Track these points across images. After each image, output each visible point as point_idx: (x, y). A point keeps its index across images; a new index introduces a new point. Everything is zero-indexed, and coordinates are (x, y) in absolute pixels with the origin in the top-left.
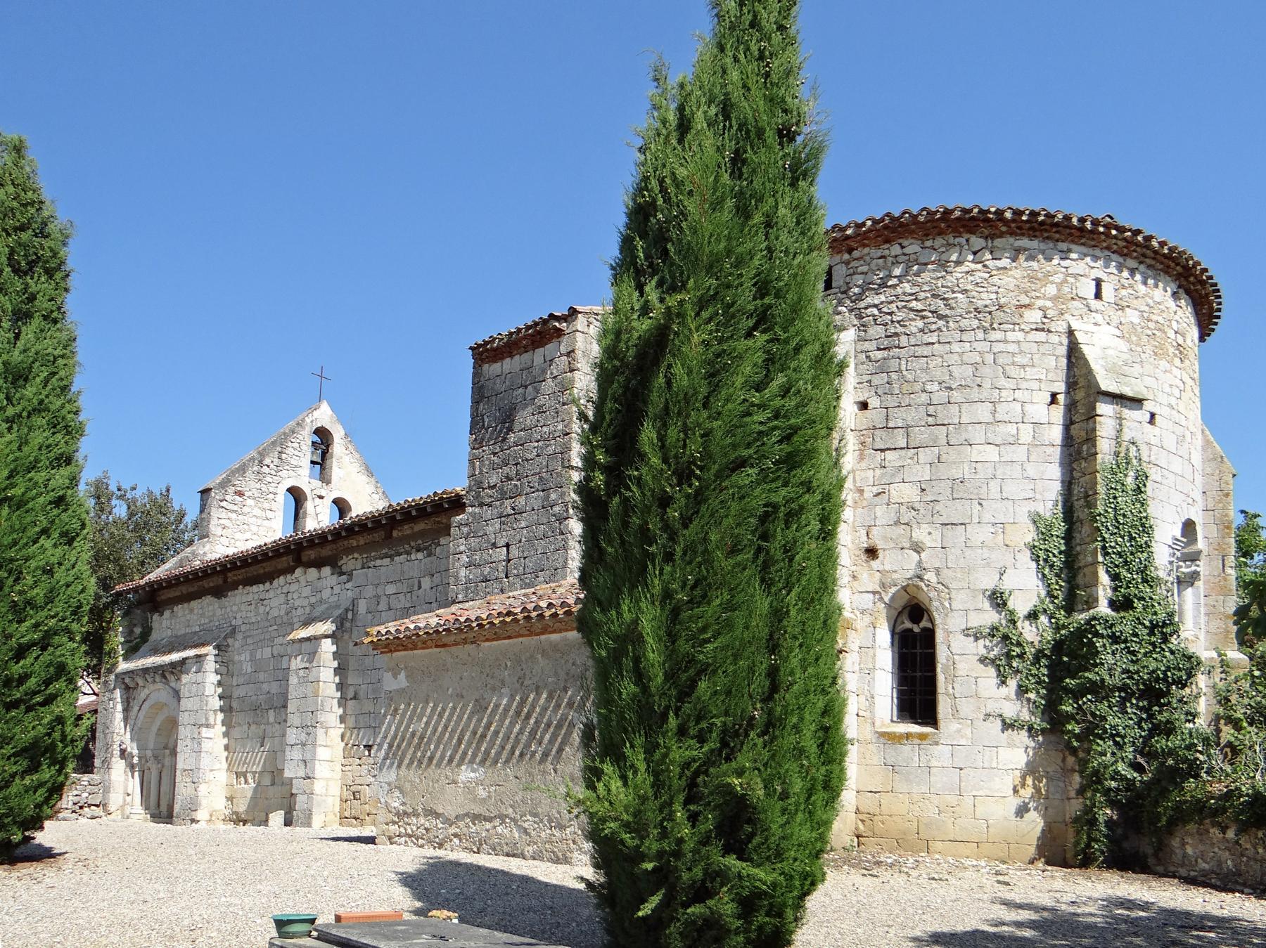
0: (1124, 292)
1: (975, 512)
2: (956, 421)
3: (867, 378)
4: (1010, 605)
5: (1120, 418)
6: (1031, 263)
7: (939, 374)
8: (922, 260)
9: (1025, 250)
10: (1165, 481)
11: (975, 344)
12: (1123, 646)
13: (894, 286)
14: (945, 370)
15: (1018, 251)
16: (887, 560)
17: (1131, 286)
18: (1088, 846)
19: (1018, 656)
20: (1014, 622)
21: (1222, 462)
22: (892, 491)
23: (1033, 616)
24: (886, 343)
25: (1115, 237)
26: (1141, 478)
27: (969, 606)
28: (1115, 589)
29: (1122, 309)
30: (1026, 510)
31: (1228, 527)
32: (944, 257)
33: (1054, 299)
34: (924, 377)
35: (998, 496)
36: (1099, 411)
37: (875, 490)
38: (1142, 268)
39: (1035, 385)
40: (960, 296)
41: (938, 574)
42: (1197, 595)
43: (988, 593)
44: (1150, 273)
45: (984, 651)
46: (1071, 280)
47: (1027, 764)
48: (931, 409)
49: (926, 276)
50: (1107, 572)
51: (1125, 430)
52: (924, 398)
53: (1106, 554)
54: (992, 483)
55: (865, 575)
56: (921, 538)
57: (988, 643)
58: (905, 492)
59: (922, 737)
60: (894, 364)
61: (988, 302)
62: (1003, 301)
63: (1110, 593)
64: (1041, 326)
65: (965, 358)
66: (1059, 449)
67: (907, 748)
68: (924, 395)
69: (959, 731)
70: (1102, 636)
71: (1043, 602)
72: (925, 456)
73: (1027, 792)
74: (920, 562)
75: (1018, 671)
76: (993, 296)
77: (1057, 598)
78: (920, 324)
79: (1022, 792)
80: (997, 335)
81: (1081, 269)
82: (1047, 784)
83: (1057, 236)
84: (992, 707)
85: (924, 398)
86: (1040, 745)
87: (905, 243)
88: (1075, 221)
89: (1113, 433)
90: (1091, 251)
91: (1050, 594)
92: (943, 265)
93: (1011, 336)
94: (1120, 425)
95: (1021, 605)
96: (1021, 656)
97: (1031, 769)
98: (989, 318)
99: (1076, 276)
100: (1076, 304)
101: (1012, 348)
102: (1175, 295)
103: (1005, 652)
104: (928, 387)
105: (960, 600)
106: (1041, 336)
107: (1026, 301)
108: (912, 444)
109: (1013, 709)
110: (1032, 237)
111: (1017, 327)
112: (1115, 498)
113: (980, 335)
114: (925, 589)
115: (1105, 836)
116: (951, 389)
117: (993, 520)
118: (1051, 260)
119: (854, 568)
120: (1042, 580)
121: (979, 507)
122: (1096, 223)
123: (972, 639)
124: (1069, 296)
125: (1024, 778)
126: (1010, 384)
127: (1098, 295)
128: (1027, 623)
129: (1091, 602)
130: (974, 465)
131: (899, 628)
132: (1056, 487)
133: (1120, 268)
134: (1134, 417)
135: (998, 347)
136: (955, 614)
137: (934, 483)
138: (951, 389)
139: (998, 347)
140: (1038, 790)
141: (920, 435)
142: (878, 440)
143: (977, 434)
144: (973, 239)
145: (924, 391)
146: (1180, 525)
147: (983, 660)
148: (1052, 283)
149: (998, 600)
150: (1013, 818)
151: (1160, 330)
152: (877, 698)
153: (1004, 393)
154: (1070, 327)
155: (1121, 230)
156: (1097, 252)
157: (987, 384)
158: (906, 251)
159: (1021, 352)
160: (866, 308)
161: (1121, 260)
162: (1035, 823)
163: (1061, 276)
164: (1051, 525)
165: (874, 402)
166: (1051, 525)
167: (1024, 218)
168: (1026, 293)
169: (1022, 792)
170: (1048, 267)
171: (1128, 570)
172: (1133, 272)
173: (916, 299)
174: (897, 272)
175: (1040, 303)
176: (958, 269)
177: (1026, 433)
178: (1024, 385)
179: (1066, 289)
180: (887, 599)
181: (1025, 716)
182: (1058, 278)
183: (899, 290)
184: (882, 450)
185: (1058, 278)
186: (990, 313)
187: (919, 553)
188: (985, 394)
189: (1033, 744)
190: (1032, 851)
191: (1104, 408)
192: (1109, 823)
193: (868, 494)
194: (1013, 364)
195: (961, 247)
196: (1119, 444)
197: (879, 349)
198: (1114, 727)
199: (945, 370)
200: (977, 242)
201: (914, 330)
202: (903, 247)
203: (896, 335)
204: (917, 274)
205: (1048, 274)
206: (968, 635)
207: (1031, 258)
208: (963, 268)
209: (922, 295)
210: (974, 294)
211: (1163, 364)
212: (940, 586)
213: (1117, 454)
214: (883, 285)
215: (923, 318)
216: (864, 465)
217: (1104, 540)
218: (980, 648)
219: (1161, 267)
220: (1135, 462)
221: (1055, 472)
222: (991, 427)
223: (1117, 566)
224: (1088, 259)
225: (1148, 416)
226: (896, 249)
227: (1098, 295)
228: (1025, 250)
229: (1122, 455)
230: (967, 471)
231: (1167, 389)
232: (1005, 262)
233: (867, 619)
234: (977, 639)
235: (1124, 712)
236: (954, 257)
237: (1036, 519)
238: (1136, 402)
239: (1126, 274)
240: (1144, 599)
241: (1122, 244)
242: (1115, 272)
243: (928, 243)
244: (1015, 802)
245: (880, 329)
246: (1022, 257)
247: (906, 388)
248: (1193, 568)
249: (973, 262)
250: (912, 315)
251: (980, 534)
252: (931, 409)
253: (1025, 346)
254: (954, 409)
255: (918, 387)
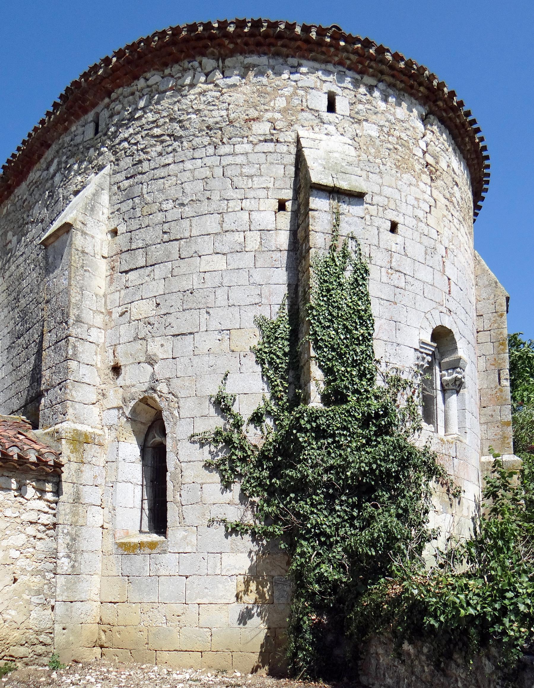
0: (361, 107)
1: (203, 320)
2: (187, 235)
3: (117, 207)
4: (235, 409)
5: (337, 215)
6: (260, 78)
7: (173, 192)
8: (162, 88)
9: (254, 66)
10: (409, 287)
11: (206, 160)
12: (330, 440)
13: (140, 118)
14: (179, 187)
15: (247, 68)
16: (128, 375)
17: (369, 102)
18: (295, 655)
19: (240, 460)
20: (237, 425)
21: (496, 287)
22: (133, 310)
23: (257, 419)
24: (132, 172)
25: (344, 49)
26: (362, 272)
27: (195, 413)
28: (328, 383)
29: (359, 122)
30: (251, 315)
31: (502, 344)
32: (180, 82)
33: (283, 111)
34: (161, 197)
35: (225, 303)
36: (312, 206)
37: (120, 310)
38: (381, 85)
39: (262, 194)
40: (193, 116)
41: (168, 385)
42: (462, 402)
43: (213, 399)
44: (391, 92)
45: (209, 457)
46: (301, 92)
47: (250, 569)
48: (166, 227)
49: (165, 103)
50: (320, 367)
51: (343, 224)
52: (160, 217)
53: (318, 348)
54: (219, 291)
55: (112, 392)
56: (155, 351)
57: (213, 449)
58: (143, 309)
59: (152, 545)
60: (137, 190)
61: (219, 119)
62: (232, 116)
63: (322, 386)
64: (268, 137)
65: (196, 173)
66: (286, 253)
67: (140, 558)
68: (160, 214)
69: (185, 538)
70: (306, 431)
71: (267, 405)
72: (159, 271)
73: (251, 598)
74: (153, 374)
75: (240, 476)
76: (224, 113)
77: (281, 399)
78: (159, 148)
79: (245, 598)
80: (224, 149)
81: (313, 83)
82: (272, 588)
83: (284, 50)
84: (217, 513)
85: (160, 217)
86: (265, 548)
87: (148, 75)
88: (298, 30)
89: (329, 228)
90: (323, 66)
91: (274, 397)
92: (178, 90)
93: (239, 148)
94: (337, 219)
95: (244, 409)
96: (243, 460)
97: (254, 574)
98: (217, 133)
99: (306, 89)
100: (306, 115)
101: (240, 159)
102: (424, 120)
103: (229, 457)
104: (164, 206)
105: (188, 407)
106: (270, 147)
107: (254, 114)
108: (150, 262)
109: (235, 513)
110: (260, 54)
111: (245, 140)
112: (328, 291)
113: (211, 150)
114: (158, 399)
115: (312, 644)
116: (182, 205)
117: (220, 327)
118: (280, 74)
119: (103, 386)
120: (267, 383)
121: (206, 316)
122: (321, 32)
123: (198, 445)
124: (299, 108)
125: (247, 583)
126: (238, 194)
127: (331, 108)
128: (252, 426)
129: (306, 400)
130: (202, 275)
131: (151, 442)
132: (284, 290)
133: (356, 84)
134: (351, 211)
135: (226, 160)
136: (183, 422)
137: (167, 296)
138: (182, 205)
139: (226, 160)
140: (261, 595)
141: (157, 252)
142: (126, 261)
143: (205, 245)
144: (205, 60)
145: (161, 210)
146: (430, 332)
147: (208, 466)
148: (281, 96)
149: (222, 406)
150: (236, 624)
151: (402, 145)
152: (118, 509)
153: (231, 204)
154: (298, 136)
155: (351, 40)
156: (330, 67)
157: (216, 197)
158: (150, 83)
159: (249, 163)
160: (119, 144)
161: (358, 77)
162: (258, 628)
163: (291, 89)
164: (276, 328)
165: (122, 229)
166: (276, 328)
167: (246, 30)
168: (255, 107)
169: (245, 598)
170: (277, 81)
171: (343, 364)
172: (371, 89)
173: (157, 127)
174: (142, 104)
175: (269, 115)
176: (192, 91)
177: (253, 241)
178: (251, 194)
179: (296, 102)
180: (127, 413)
181: (249, 519)
182: (287, 91)
183: (144, 121)
184: (126, 272)
185: (287, 91)
186: (220, 129)
187: (152, 365)
188: (214, 206)
189: (257, 548)
190: (255, 658)
191: (319, 203)
192: (316, 628)
193: (115, 315)
194: (241, 174)
195: (195, 70)
196: (335, 238)
197: (127, 178)
198: (317, 525)
199: (179, 187)
200: (209, 63)
201: (154, 154)
202: (147, 80)
203: (140, 162)
204: (158, 103)
205: (278, 88)
206: (194, 442)
207: (261, 73)
208: (197, 90)
209: (162, 121)
210: (206, 112)
211: (407, 177)
212: (170, 396)
213: (333, 248)
214: (132, 118)
215: (162, 142)
216: (113, 288)
217: (315, 333)
218: (205, 454)
219: (402, 85)
220: (353, 256)
221: (282, 276)
222: (219, 237)
223: (329, 360)
224: (320, 73)
225: (389, 224)
226: (141, 83)
227: (331, 108)
228: (254, 66)
229: (339, 249)
230: (195, 282)
231: (412, 201)
232: (235, 79)
233: (114, 434)
234: (202, 445)
235: (332, 511)
236: (188, 81)
237: (261, 323)
238: (357, 197)
239: (362, 90)
240: (360, 393)
241: (354, 57)
242: (350, 86)
243: (167, 71)
244: (238, 609)
245: (129, 160)
246: (251, 74)
247: (146, 209)
248: (455, 375)
249: (206, 82)
250: (153, 142)
251: (207, 341)
252: (166, 227)
253: (253, 158)
254: (185, 223)
255: (155, 207)
